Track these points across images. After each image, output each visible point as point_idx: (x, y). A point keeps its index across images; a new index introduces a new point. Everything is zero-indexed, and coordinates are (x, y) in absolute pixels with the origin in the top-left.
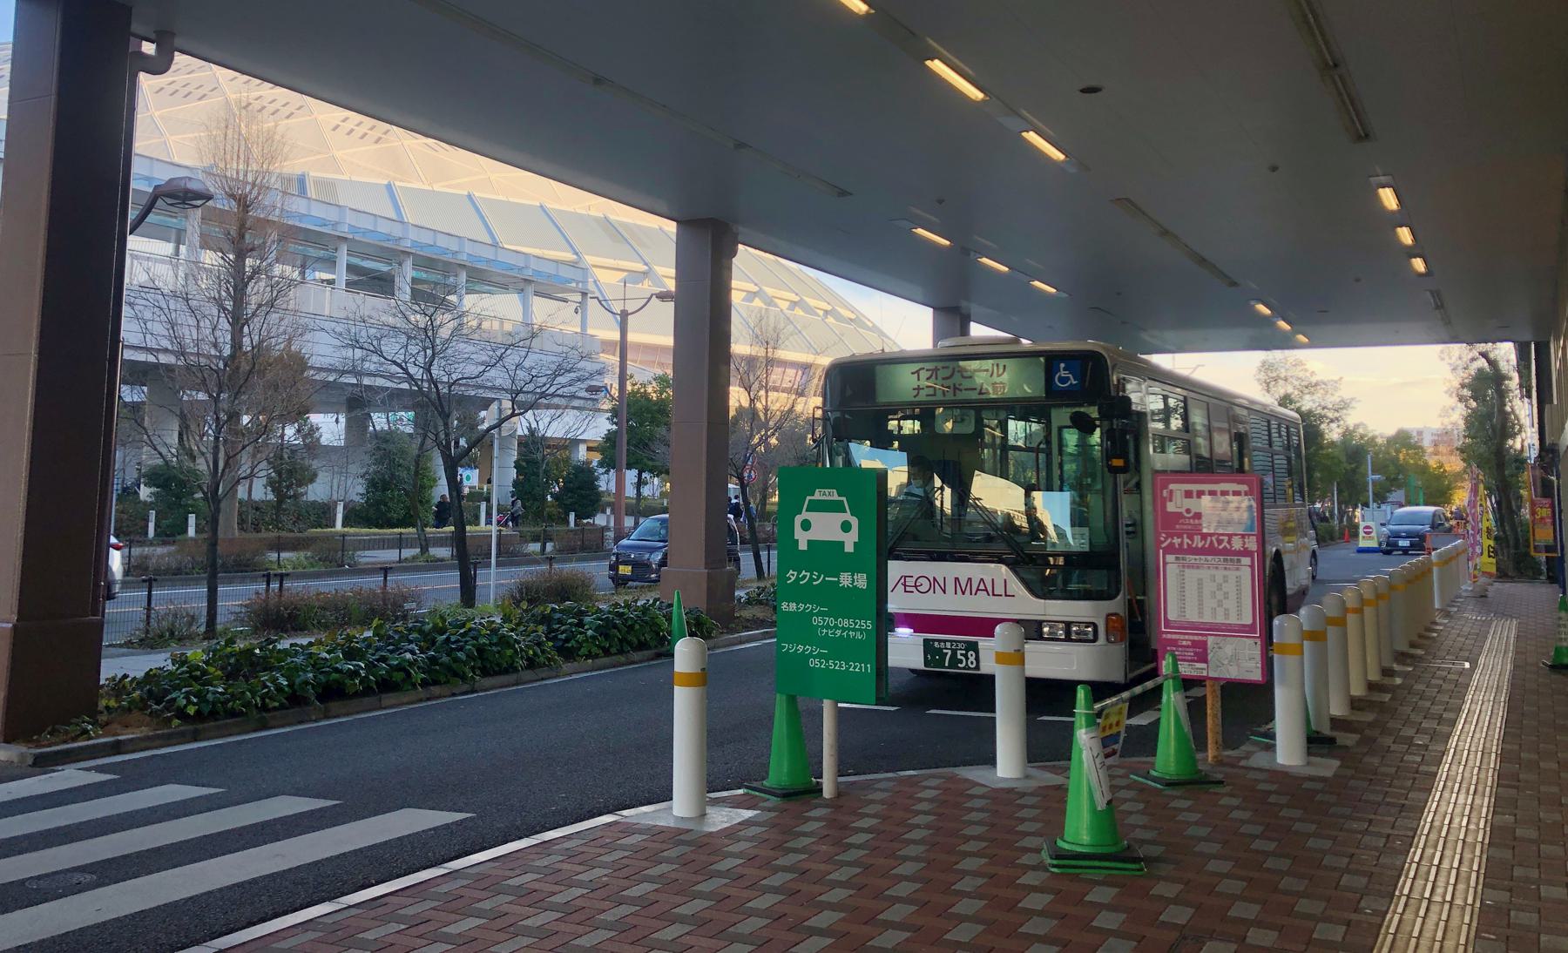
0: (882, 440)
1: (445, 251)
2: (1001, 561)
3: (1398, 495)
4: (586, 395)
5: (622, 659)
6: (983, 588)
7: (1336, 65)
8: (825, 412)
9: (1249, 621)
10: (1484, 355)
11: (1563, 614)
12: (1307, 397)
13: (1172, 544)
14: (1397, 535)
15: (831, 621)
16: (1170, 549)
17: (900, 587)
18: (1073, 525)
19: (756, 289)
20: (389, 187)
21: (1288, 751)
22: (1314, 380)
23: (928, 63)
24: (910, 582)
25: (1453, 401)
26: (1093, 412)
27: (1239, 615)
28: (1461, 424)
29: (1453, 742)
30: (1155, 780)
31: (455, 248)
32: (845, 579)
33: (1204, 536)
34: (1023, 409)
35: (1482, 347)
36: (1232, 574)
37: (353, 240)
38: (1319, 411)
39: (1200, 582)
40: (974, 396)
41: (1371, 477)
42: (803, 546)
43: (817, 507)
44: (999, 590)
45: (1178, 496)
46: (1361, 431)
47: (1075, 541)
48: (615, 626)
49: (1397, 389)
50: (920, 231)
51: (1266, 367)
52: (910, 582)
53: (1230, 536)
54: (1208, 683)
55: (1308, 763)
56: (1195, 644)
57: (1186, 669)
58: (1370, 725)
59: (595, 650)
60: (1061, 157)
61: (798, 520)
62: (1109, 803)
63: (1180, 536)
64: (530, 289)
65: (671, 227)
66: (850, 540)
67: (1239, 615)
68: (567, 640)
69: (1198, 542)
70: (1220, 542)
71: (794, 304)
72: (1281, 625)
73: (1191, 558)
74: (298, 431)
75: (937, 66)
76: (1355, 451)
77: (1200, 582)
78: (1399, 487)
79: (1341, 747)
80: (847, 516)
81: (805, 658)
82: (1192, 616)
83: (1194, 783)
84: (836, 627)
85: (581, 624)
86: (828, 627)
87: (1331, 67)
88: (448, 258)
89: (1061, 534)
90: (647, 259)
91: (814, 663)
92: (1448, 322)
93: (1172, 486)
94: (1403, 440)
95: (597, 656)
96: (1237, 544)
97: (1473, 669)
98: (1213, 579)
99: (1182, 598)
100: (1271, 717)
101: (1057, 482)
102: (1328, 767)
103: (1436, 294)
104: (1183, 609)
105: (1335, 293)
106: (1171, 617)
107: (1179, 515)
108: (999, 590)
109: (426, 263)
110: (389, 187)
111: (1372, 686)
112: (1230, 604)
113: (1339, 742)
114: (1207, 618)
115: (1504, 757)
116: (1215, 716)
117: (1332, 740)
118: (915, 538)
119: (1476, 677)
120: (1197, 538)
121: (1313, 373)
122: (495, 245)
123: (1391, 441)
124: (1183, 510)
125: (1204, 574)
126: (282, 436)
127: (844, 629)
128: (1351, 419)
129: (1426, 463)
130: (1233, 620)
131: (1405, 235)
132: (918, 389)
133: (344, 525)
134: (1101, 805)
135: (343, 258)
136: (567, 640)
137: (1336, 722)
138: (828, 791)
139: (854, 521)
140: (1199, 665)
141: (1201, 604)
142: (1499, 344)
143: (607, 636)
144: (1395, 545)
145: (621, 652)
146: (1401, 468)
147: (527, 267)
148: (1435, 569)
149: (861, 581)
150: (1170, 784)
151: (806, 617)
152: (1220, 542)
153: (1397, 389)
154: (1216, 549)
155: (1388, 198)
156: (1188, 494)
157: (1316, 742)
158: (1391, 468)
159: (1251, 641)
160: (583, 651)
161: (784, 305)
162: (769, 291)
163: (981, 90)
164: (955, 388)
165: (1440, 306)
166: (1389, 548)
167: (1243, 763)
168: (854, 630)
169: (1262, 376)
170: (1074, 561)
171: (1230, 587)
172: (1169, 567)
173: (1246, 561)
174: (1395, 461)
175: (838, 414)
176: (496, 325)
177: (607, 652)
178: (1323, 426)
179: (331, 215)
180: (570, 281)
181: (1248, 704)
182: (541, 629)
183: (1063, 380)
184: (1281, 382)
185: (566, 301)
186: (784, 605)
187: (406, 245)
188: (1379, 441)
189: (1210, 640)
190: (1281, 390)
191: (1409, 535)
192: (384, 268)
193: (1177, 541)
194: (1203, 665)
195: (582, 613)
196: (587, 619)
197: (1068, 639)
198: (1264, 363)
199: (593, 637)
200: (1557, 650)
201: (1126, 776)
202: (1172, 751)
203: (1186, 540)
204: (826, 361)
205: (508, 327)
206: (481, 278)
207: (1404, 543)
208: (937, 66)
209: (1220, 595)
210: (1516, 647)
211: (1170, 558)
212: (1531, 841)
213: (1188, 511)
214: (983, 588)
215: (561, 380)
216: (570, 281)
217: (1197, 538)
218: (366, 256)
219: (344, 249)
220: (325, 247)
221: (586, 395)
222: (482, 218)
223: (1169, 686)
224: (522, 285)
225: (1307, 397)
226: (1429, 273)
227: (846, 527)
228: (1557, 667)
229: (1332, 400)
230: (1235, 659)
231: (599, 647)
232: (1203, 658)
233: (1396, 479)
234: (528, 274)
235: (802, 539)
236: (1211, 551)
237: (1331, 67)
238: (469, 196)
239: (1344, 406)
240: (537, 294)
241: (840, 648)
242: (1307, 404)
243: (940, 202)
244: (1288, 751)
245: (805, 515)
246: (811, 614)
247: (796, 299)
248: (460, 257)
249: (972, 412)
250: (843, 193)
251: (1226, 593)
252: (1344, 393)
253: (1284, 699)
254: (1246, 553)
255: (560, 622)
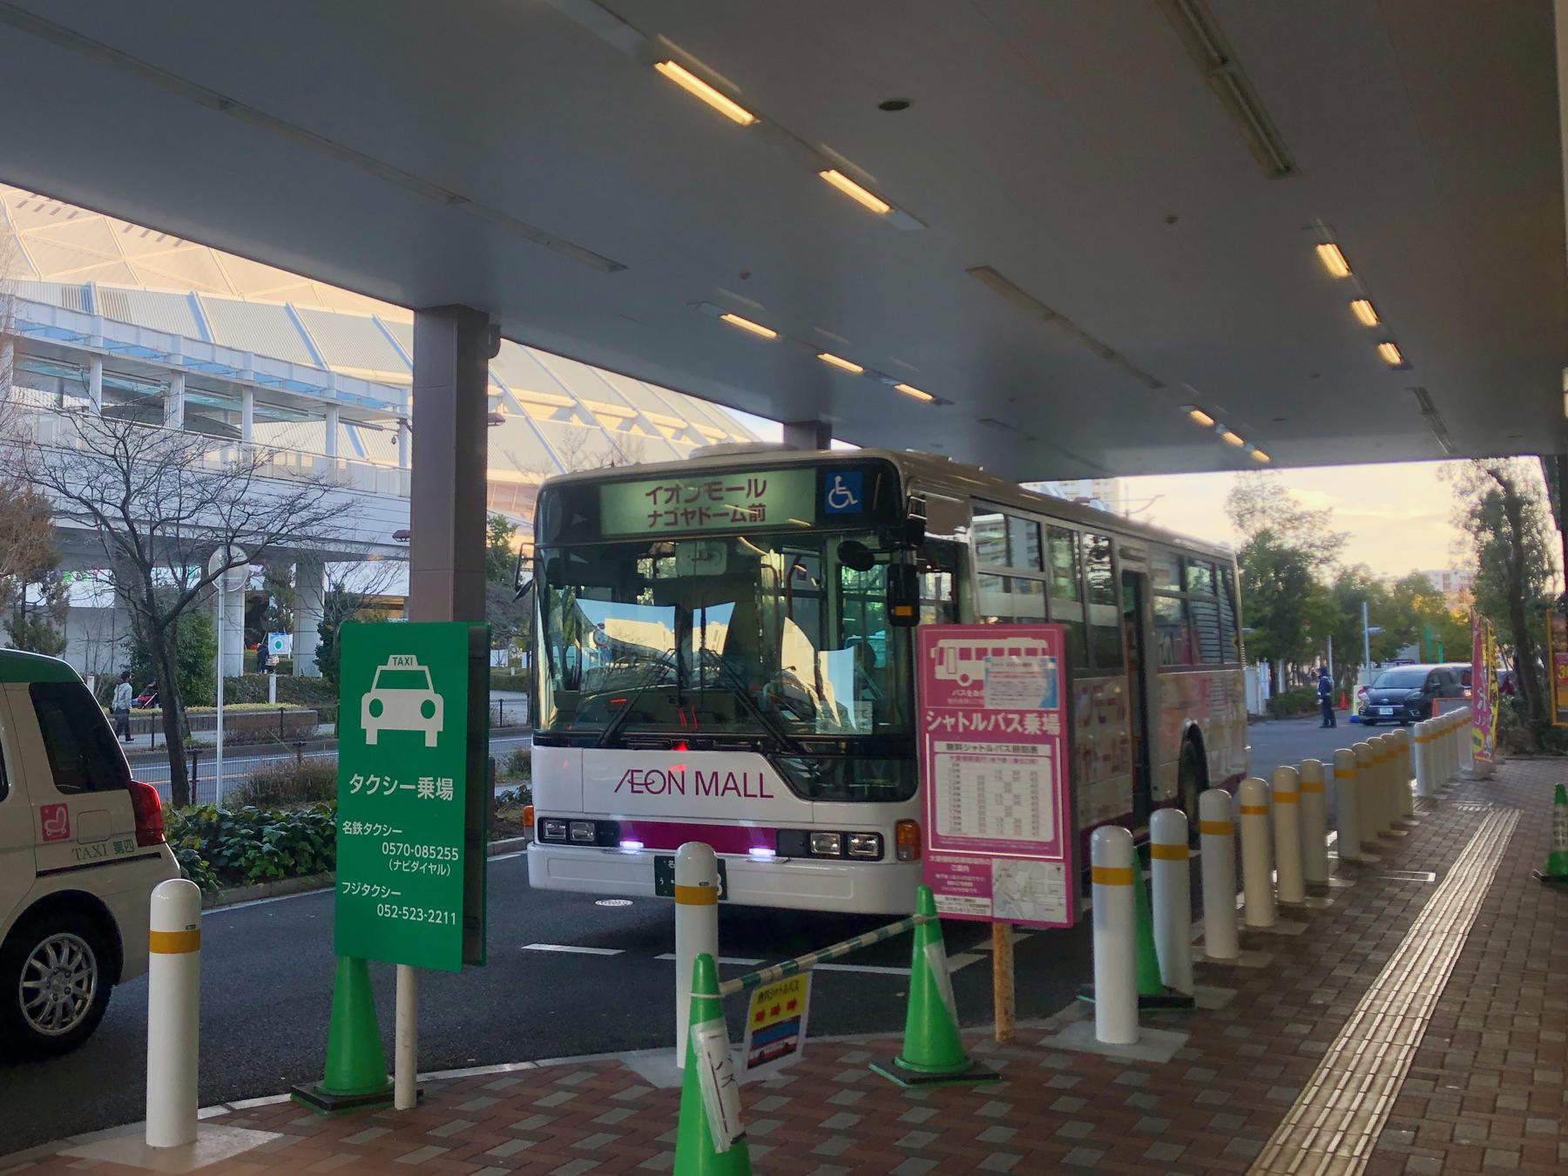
0: (625, 589)
1: (227, 370)
2: (754, 749)
3: (1411, 651)
4: (394, 542)
5: (311, 880)
6: (733, 785)
7: (1224, 61)
8: (537, 549)
9: (1047, 836)
10: (1494, 473)
11: (1561, 808)
12: (1290, 533)
13: (942, 726)
14: (1377, 701)
15: (404, 847)
16: (941, 733)
17: (626, 785)
18: (856, 698)
19: (634, 414)
20: (191, 299)
21: (1111, 1021)
22: (1298, 511)
23: (659, 66)
24: (639, 778)
25: (1458, 533)
26: (871, 542)
27: (1035, 828)
28: (1475, 560)
29: (1365, 1003)
30: (898, 1072)
31: (239, 366)
32: (425, 787)
33: (986, 715)
34: (778, 538)
35: (1491, 463)
36: (1025, 769)
37: (109, 357)
38: (1305, 549)
39: (981, 780)
40: (725, 523)
41: (1368, 630)
42: (372, 739)
43: (395, 681)
44: (753, 788)
45: (951, 656)
46: (1362, 573)
47: (857, 722)
48: (306, 838)
49: (1393, 519)
50: (731, 318)
51: (1240, 496)
52: (639, 778)
53: (1022, 713)
54: (995, 926)
55: (1140, 1040)
56: (975, 870)
57: (948, 905)
58: (1260, 974)
59: (271, 870)
60: (884, 208)
61: (366, 700)
62: (736, 1141)
63: (953, 714)
64: (335, 415)
65: (406, 317)
66: (432, 729)
67: (1035, 828)
68: (235, 857)
69: (978, 723)
70: (1008, 722)
71: (628, 423)
72: (1101, 843)
73: (969, 747)
74: (44, 590)
75: (672, 70)
76: (1353, 598)
77: (981, 780)
78: (1412, 642)
79: (1202, 1010)
80: (429, 694)
81: (372, 902)
82: (970, 830)
83: (960, 1075)
84: (412, 858)
85: (259, 836)
86: (401, 858)
87: (1216, 61)
88: (232, 378)
89: (843, 712)
90: (574, 393)
91: (383, 910)
92: (1441, 431)
93: (942, 643)
94: (1418, 584)
95: (275, 878)
96: (1032, 725)
97: (1438, 881)
98: (999, 776)
99: (957, 807)
100: (1091, 979)
101: (834, 640)
102: (1168, 1043)
103: (1422, 393)
104: (957, 820)
105: (1303, 402)
106: (941, 831)
107: (951, 685)
108: (753, 788)
109: (198, 383)
110: (191, 299)
111: (1285, 911)
112: (1023, 812)
113: (1199, 1003)
114: (991, 833)
115: (1433, 1027)
116: (1004, 974)
117: (1188, 1002)
118: (648, 718)
119: (1437, 895)
120: (977, 717)
121: (1296, 503)
122: (320, 369)
123: (1401, 586)
124: (957, 677)
125: (986, 768)
126: (23, 596)
127: (422, 861)
128: (1347, 558)
129: (1447, 613)
130: (1027, 835)
131: (1364, 312)
132: (656, 515)
133: (278, 700)
134: (722, 1143)
135: (97, 379)
136: (235, 857)
137: (1208, 972)
138: (402, 1099)
139: (439, 702)
140: (979, 901)
141: (982, 813)
142: (1513, 459)
143: (293, 852)
144: (1374, 713)
145: (312, 871)
146: (1415, 620)
147: (329, 388)
148: (1417, 747)
149: (446, 789)
150: (916, 1080)
151: (374, 842)
152: (1008, 722)
153: (1393, 519)
154: (1003, 733)
155: (1332, 259)
156: (965, 654)
157: (1154, 1005)
158: (1401, 618)
159: (1052, 866)
160: (255, 871)
161: (668, 433)
162: (590, 405)
163: (749, 111)
164: (702, 514)
165: (1429, 410)
166: (1370, 718)
167: (1046, 1041)
168: (436, 862)
169: (1233, 507)
170: (858, 747)
171: (1022, 787)
172: (938, 758)
173: (1044, 749)
174: (1406, 609)
175: (556, 554)
176: (292, 461)
177: (291, 872)
178: (1311, 569)
179: (125, 336)
180: (385, 405)
181: (1056, 958)
182: (200, 843)
183: (839, 499)
184: (1258, 514)
185: (380, 429)
186: (346, 826)
187: (177, 362)
188: (1389, 588)
189: (996, 863)
190: (1258, 524)
191: (1392, 701)
192: (154, 391)
193: (949, 721)
194: (986, 901)
195: (264, 821)
196: (268, 829)
197: (845, 854)
198: (1237, 491)
199: (270, 853)
200: (1554, 856)
201: (864, 1066)
202: (926, 1031)
203: (962, 721)
204: (539, 480)
205: (307, 462)
206: (283, 403)
207: (1385, 711)
208: (672, 70)
209: (1008, 799)
210: (1509, 848)
211: (940, 746)
212: (1516, 1113)
213: (965, 678)
214: (733, 785)
215: (294, 519)
216: (385, 405)
217: (977, 717)
218: (129, 376)
219: (98, 369)
220: (156, 383)
221: (394, 542)
222: (303, 334)
223: (922, 934)
224: (324, 410)
225: (1290, 533)
226: (1405, 365)
227: (428, 710)
228: (1553, 880)
229: (1319, 535)
230: (1029, 891)
231: (277, 866)
232: (985, 890)
233: (1406, 632)
234: (331, 396)
235: (371, 727)
236: (995, 735)
237: (1216, 61)
238: (287, 308)
239: (1335, 542)
240: (343, 420)
241: (416, 889)
242: (1290, 541)
243: (745, 276)
244: (1111, 1021)
245: (375, 693)
246: (381, 839)
247: (683, 425)
248: (246, 376)
249: (724, 547)
250: (615, 267)
251: (1017, 797)
252: (1336, 527)
253: (1109, 952)
254: (1045, 738)
255: (231, 833)
